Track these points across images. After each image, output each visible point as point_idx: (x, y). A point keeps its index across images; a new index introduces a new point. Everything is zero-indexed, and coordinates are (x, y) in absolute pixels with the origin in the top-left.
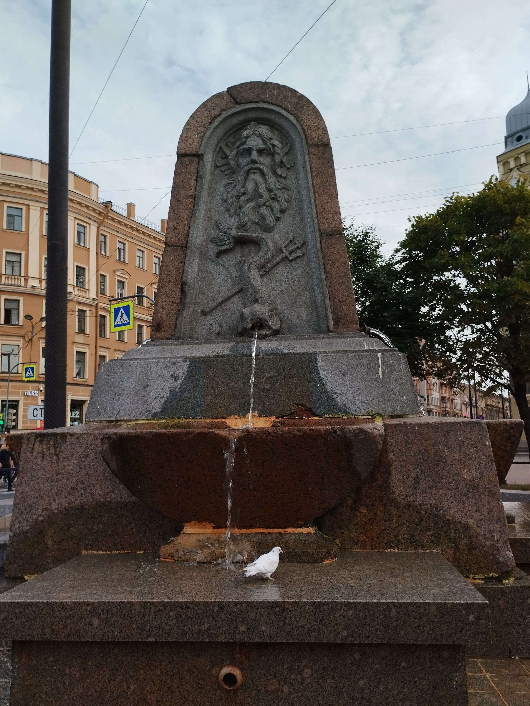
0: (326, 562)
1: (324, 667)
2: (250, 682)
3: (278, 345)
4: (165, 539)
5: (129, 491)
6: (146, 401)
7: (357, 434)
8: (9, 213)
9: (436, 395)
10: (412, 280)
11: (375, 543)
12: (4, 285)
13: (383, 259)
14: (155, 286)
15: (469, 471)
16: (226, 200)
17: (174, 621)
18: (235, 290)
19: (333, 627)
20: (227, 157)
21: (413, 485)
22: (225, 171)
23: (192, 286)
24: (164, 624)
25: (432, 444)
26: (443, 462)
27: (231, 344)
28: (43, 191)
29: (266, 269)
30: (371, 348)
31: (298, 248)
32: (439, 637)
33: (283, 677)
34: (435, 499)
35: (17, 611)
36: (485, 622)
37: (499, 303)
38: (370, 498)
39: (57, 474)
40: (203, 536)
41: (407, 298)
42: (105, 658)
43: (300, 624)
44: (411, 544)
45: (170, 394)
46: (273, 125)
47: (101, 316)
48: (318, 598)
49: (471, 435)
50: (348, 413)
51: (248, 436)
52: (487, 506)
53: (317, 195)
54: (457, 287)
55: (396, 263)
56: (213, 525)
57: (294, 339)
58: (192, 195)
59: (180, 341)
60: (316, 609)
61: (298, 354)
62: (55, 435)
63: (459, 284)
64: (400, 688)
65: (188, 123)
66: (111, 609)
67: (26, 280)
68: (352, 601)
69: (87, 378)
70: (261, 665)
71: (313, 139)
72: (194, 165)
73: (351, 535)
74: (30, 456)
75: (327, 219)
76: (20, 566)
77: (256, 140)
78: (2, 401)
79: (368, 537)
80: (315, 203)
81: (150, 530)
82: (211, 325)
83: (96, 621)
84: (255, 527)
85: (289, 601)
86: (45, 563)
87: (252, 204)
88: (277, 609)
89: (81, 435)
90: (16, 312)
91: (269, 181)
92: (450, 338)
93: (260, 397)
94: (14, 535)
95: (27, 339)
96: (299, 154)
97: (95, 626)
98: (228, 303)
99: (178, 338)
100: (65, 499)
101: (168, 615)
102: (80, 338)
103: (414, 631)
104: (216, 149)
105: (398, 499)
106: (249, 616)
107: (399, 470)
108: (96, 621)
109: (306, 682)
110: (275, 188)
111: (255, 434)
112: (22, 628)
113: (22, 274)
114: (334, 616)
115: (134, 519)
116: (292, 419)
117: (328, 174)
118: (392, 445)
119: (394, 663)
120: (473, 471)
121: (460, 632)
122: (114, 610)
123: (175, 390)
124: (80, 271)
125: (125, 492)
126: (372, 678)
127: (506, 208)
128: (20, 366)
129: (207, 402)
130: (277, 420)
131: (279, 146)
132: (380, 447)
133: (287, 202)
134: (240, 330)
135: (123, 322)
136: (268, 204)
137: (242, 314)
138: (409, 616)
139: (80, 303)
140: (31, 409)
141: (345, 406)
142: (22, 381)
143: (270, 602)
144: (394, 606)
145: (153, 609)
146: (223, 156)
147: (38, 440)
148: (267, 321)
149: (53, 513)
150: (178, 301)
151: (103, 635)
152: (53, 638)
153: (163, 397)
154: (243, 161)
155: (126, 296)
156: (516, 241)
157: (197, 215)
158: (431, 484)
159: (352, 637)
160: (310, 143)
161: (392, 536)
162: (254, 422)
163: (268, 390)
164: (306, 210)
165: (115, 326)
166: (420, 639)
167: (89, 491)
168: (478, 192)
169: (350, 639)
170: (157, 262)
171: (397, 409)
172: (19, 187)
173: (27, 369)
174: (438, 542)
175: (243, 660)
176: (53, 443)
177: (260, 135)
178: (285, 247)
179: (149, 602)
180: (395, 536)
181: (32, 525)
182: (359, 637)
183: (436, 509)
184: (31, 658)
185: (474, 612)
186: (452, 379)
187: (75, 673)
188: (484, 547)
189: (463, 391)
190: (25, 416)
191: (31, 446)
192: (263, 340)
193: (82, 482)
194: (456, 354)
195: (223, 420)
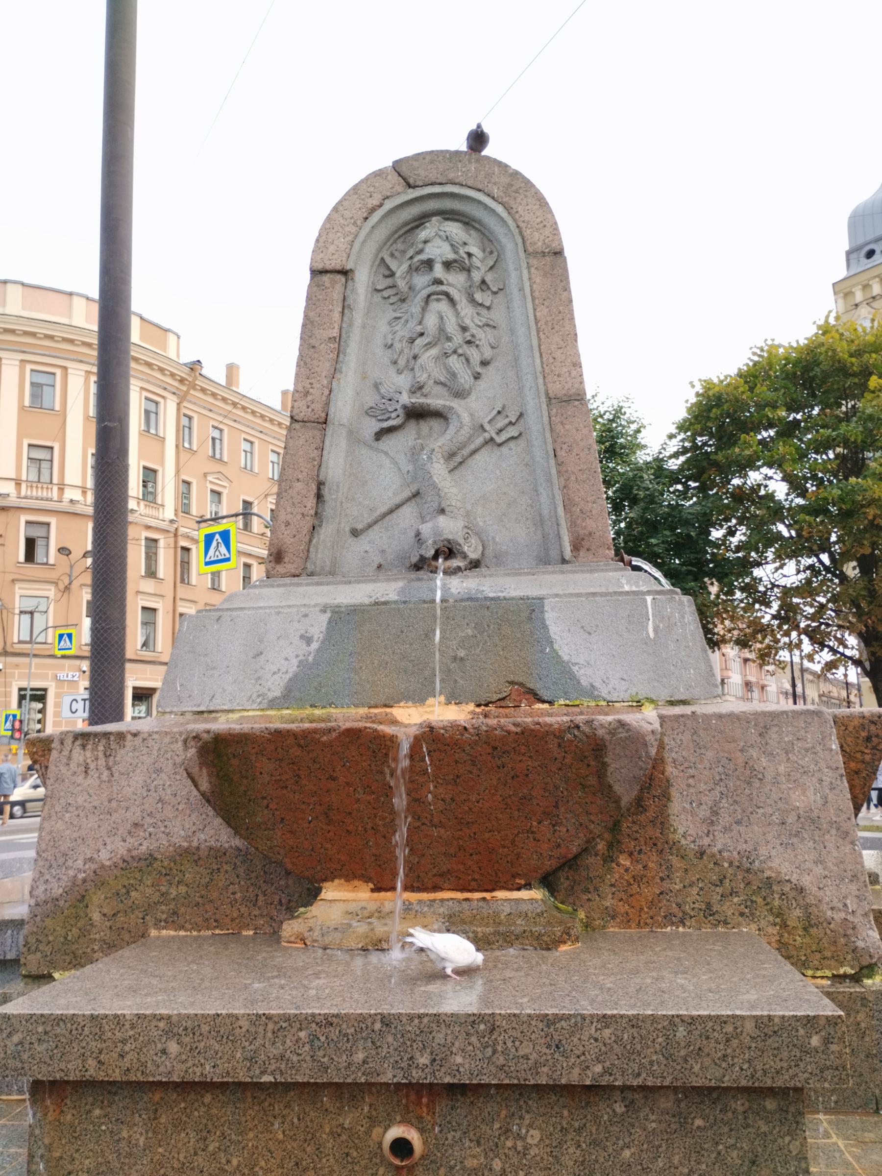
0: (563, 948)
1: (562, 1128)
2: (436, 1152)
3: (479, 585)
4: (290, 909)
5: (229, 829)
6: (259, 678)
7: (615, 729)
8: (34, 380)
9: (736, 678)
10: (697, 484)
11: (644, 916)
12: (26, 498)
13: (647, 451)
14: (272, 499)
15: (804, 792)
16: (392, 345)
17: (307, 1048)
18: (407, 493)
19: (578, 1057)
20: (392, 275)
21: (709, 818)
22: (389, 297)
23: (335, 488)
24: (288, 1052)
25: (740, 748)
26: (759, 779)
27: (401, 584)
28: (89, 345)
29: (458, 459)
30: (634, 589)
31: (511, 423)
32: (760, 1073)
33: (491, 1144)
34: (746, 842)
35: (40, 1029)
36: (838, 1049)
37: (846, 516)
38: (636, 839)
39: (110, 801)
40: (354, 904)
41: (689, 513)
42: (188, 1110)
43: (521, 1053)
44: (706, 918)
45: (298, 667)
46: (467, 222)
47: (183, 548)
48: (551, 1007)
49: (806, 732)
50: (596, 698)
51: (431, 737)
52: (835, 853)
53: (542, 336)
54: (770, 497)
55: (670, 457)
56: (371, 886)
57: (505, 575)
58: (335, 338)
59: (315, 579)
60: (548, 1026)
61: (513, 599)
62: (106, 735)
63: (774, 491)
64: (693, 1163)
65: (329, 219)
66: (199, 1026)
67: (61, 490)
68: (609, 1012)
69: (160, 650)
70: (454, 1124)
71: (535, 244)
72: (339, 287)
73: (604, 903)
74: (64, 770)
75: (559, 376)
76: (46, 956)
77: (443, 234)
78: (20, 689)
79: (633, 907)
80: (540, 349)
81: (265, 895)
82: (366, 552)
83: (173, 1047)
84: (442, 889)
85: (503, 1012)
86: (89, 950)
87: (434, 352)
88: (482, 1027)
89: (150, 735)
90: (44, 543)
91: (462, 314)
92: (761, 580)
93: (449, 670)
94: (37, 905)
95: (62, 587)
96: (511, 267)
97: (173, 1056)
98: (394, 515)
99: (311, 574)
100: (122, 843)
101: (296, 1037)
102: (148, 585)
103: (716, 1064)
104: (374, 262)
105: (683, 842)
106: (434, 1038)
107: (685, 793)
108: (173, 1047)
109: (532, 1153)
110: (472, 324)
111: (442, 731)
112: (48, 1060)
113: (55, 481)
114: (579, 1039)
115: (238, 876)
116: (503, 707)
117: (561, 300)
118: (671, 750)
119: (682, 1120)
120: (810, 793)
121: (795, 1066)
122: (205, 1028)
123: (307, 660)
124: (150, 475)
125: (222, 831)
126: (645, 1146)
127: (853, 364)
128: (50, 631)
129: (361, 679)
130: (478, 710)
131: (478, 256)
132: (653, 751)
133: (493, 348)
134: (415, 559)
135: (220, 557)
136: (460, 351)
137: (418, 534)
138: (707, 1038)
139: (148, 527)
140: (67, 700)
141: (592, 686)
142: (53, 656)
143: (470, 1015)
144: (683, 1021)
145: (271, 1026)
146: (387, 273)
147: (79, 742)
148: (460, 545)
149: (103, 867)
150: (312, 512)
151: (186, 1071)
152: (101, 1076)
153: (286, 672)
154: (421, 280)
155: (225, 514)
156: (871, 418)
157: (344, 369)
158: (740, 817)
159: (611, 1075)
160: (530, 250)
161: (674, 905)
162: (443, 713)
163: (462, 659)
164: (525, 362)
165: (207, 564)
166: (727, 1078)
167: (163, 829)
168: (806, 339)
169: (607, 1078)
170: (276, 460)
171: (679, 691)
172: (51, 338)
173: (61, 636)
174: (752, 914)
175: (424, 1115)
176: (102, 748)
177: (447, 238)
178: (490, 422)
179: (264, 1014)
180: (679, 906)
181: (66, 887)
182: (623, 1075)
183: (748, 858)
184: (62, 1112)
185: (820, 1030)
186: (765, 649)
187: (138, 1136)
188: (830, 924)
189: (783, 669)
190: (57, 714)
191: (66, 753)
192: (453, 577)
193: (150, 815)
194: (770, 607)
195: (388, 710)
